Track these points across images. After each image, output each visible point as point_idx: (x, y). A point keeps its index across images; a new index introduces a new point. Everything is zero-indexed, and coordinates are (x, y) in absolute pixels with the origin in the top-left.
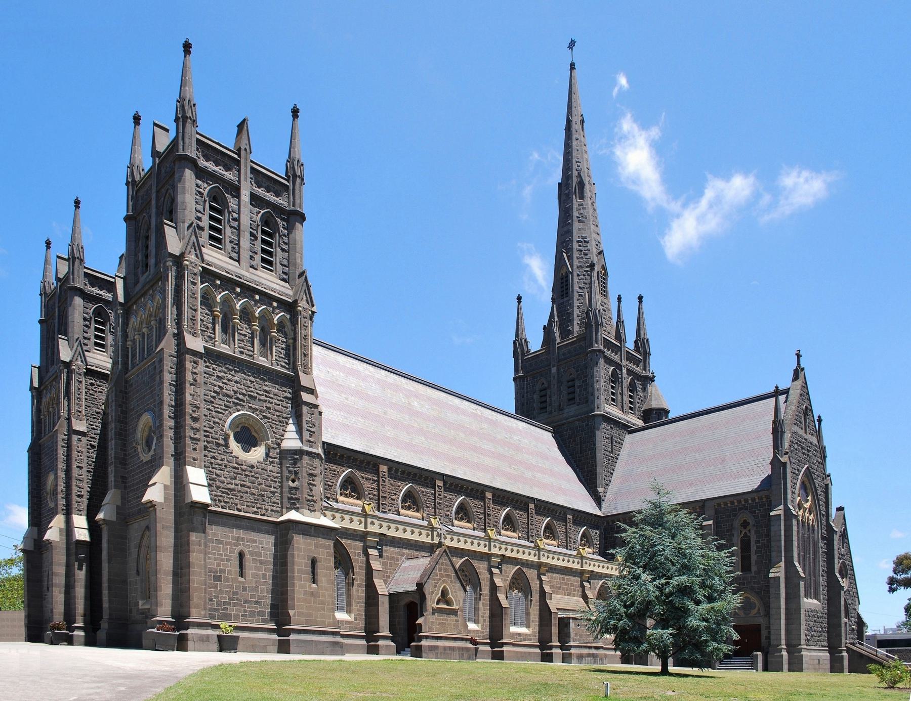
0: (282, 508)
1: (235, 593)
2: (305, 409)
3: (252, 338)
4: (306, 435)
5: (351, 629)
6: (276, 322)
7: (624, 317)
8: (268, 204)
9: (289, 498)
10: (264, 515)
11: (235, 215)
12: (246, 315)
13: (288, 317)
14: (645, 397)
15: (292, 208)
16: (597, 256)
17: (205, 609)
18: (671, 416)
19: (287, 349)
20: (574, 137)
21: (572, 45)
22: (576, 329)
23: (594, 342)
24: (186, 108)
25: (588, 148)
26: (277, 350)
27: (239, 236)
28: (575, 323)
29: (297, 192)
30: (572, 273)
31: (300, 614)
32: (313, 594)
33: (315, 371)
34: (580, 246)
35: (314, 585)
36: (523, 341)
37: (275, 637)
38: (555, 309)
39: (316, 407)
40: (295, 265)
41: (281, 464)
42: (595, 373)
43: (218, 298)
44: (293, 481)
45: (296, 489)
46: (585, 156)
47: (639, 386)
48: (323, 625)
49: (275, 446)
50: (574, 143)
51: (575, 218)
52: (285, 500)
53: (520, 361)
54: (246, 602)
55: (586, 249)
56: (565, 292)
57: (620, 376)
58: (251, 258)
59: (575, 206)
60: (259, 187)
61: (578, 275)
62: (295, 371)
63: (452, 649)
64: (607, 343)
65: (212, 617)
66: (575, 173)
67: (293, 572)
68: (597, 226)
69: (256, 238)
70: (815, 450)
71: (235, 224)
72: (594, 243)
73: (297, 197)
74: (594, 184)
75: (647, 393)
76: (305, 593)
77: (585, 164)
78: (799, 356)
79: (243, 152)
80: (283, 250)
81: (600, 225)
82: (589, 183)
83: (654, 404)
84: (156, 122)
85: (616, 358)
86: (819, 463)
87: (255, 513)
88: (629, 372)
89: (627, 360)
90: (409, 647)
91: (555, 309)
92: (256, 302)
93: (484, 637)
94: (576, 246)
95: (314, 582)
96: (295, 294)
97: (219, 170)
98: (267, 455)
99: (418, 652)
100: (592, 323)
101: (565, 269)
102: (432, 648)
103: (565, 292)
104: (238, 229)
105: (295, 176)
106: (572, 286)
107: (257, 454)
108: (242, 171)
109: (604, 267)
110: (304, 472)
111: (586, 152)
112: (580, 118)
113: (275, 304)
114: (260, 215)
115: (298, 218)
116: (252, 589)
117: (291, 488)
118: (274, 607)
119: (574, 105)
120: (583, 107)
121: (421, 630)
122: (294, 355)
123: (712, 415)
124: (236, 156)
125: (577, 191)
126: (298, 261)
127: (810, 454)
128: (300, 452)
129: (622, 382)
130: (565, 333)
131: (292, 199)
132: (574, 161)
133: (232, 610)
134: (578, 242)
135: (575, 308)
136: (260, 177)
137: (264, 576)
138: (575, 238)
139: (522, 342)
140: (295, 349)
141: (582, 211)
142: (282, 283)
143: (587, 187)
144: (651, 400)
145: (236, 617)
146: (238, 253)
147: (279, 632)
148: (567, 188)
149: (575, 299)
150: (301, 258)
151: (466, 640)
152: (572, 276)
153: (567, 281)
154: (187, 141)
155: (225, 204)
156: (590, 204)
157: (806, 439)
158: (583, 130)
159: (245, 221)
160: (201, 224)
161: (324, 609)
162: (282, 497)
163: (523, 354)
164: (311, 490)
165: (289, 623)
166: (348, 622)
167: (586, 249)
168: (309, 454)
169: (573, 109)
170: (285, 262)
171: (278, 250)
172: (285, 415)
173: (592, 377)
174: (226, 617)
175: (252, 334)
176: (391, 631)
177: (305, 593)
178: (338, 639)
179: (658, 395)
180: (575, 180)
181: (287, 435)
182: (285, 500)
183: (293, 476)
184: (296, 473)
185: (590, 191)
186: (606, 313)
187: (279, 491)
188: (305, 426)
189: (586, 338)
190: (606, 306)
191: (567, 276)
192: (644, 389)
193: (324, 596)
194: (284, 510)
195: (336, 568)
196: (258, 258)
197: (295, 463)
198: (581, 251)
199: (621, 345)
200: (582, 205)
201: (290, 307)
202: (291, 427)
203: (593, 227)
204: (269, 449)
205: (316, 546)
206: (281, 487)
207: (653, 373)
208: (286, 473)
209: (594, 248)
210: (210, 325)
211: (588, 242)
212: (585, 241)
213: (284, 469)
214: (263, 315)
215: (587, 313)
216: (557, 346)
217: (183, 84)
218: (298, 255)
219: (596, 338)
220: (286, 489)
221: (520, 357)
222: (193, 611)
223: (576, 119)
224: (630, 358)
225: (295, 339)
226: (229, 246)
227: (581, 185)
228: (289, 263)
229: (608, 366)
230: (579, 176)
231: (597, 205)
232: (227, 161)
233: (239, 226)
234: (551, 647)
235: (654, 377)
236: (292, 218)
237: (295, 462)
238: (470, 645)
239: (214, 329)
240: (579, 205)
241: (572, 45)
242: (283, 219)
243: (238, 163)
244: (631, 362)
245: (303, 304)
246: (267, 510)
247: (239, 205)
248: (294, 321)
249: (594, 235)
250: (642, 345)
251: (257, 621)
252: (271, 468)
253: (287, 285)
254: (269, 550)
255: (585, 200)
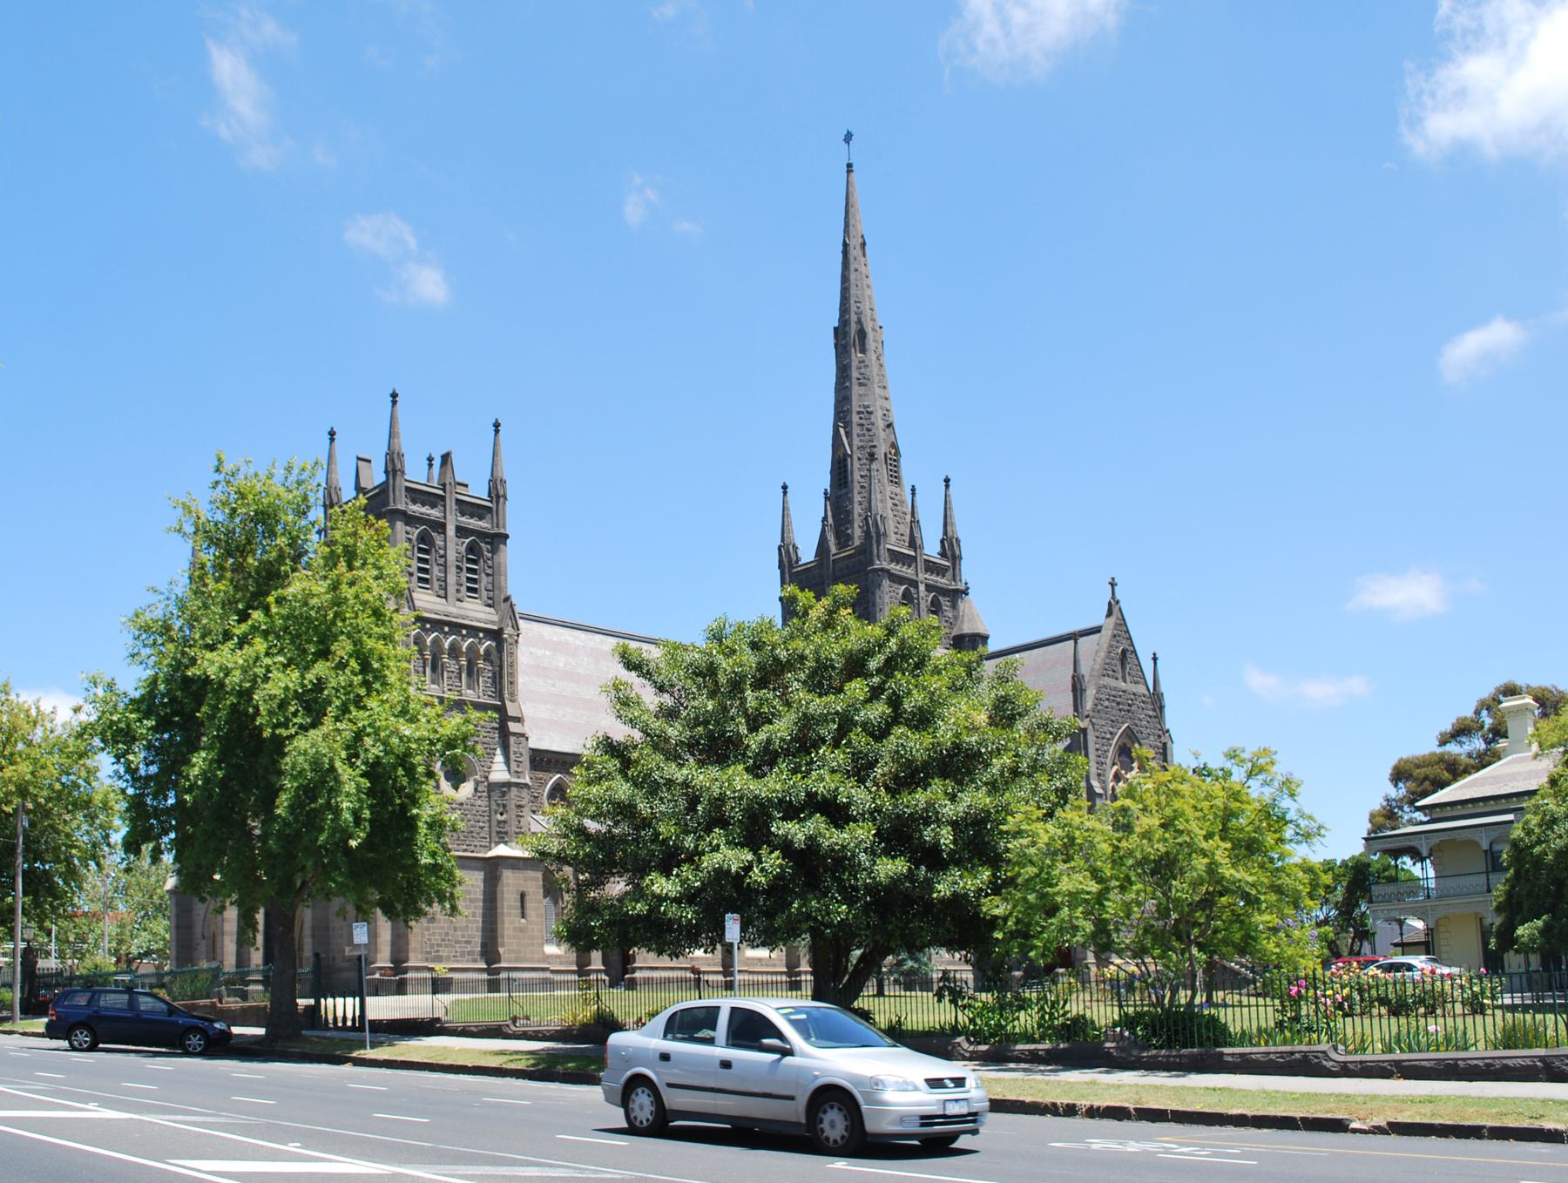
0: (490, 842)
1: (447, 934)
2: (512, 739)
3: (460, 674)
4: (514, 766)
5: (561, 963)
6: (482, 653)
7: (921, 516)
8: (471, 532)
9: (498, 833)
10: (473, 852)
11: (442, 552)
12: (454, 651)
13: (494, 644)
14: (956, 618)
15: (496, 531)
16: (884, 430)
17: (422, 953)
18: (992, 646)
19: (494, 677)
20: (852, 267)
21: (848, 138)
22: (857, 532)
23: (875, 558)
24: (396, 461)
25: (871, 281)
26: (484, 681)
27: (446, 572)
28: (856, 526)
29: (501, 512)
30: (851, 456)
31: (510, 951)
32: (522, 930)
33: (521, 697)
34: (861, 418)
35: (523, 921)
36: (791, 547)
37: (485, 976)
38: (829, 508)
39: (523, 735)
40: (500, 588)
41: (489, 797)
42: (878, 600)
43: (429, 641)
44: (502, 814)
45: (505, 822)
46: (868, 292)
47: (945, 602)
48: (532, 960)
49: (483, 779)
50: (853, 276)
51: (854, 381)
52: (494, 834)
53: (787, 576)
54: (457, 942)
55: (869, 422)
56: (843, 481)
57: (915, 596)
58: (458, 591)
59: (855, 364)
60: (463, 516)
61: (859, 459)
62: (503, 701)
63: (669, 981)
64: (896, 557)
65: (427, 960)
66: (854, 318)
67: (503, 908)
68: (884, 388)
69: (461, 569)
70: (1143, 702)
71: (441, 561)
72: (879, 413)
73: (501, 518)
74: (881, 327)
75: (958, 612)
76: (515, 929)
77: (868, 304)
78: (1113, 585)
79: (448, 487)
80: (488, 575)
81: (890, 386)
82: (873, 330)
83: (967, 629)
84: (360, 456)
85: (908, 572)
86: (1150, 717)
87: (465, 850)
88: (929, 588)
89: (927, 571)
90: (623, 980)
91: (829, 508)
92: (463, 636)
93: (714, 965)
94: (855, 418)
95: (523, 917)
96: (501, 620)
97: (425, 510)
98: (476, 790)
99: (632, 985)
100: (873, 534)
101: (842, 450)
102: (648, 982)
103: (843, 481)
104: (445, 565)
105: (498, 497)
106: (852, 474)
107: (467, 789)
108: (448, 507)
109: (894, 446)
110: (512, 806)
111: (868, 286)
112: (860, 240)
113: (481, 635)
114: (465, 545)
115: (502, 539)
116: (462, 929)
117: (499, 822)
118: (483, 945)
119: (852, 222)
120: (865, 224)
121: (634, 962)
122: (501, 683)
123: (1035, 651)
124: (441, 492)
125: (857, 342)
126: (503, 584)
127: (1133, 708)
128: (508, 785)
129: (918, 604)
130: (843, 538)
131: (495, 520)
132: (852, 302)
133: (444, 952)
134: (859, 413)
135: (856, 505)
136: (466, 508)
137: (474, 915)
138: (855, 408)
139: (789, 549)
140: (501, 677)
141: (863, 370)
142: (488, 609)
143: (870, 335)
144: (962, 622)
145: (448, 959)
146: (446, 589)
147: (489, 971)
148: (845, 338)
149: (856, 491)
150: (506, 580)
151: (686, 969)
152: (852, 459)
153: (846, 466)
154: (397, 493)
155: (431, 543)
156: (874, 358)
157: (1124, 691)
158: (864, 255)
159: (452, 556)
160: (410, 570)
161: (533, 944)
162: (490, 832)
163: (791, 566)
164: (519, 822)
165: (499, 961)
166: (558, 956)
167: (869, 422)
168: (517, 785)
169: (851, 228)
170: (490, 587)
171: (483, 575)
172: (492, 746)
173: (874, 604)
174: (439, 959)
175: (460, 669)
176: (604, 964)
177: (515, 929)
178: (548, 975)
179: (972, 614)
180: (854, 327)
181: (495, 767)
182: (494, 834)
183: (501, 810)
184: (504, 806)
185: (875, 341)
186: (899, 508)
187: (487, 825)
188: (512, 757)
189: (865, 553)
190: (898, 497)
191: (845, 460)
192: (954, 606)
193: (533, 930)
194: (493, 845)
195: (545, 897)
196: (463, 589)
197: (504, 796)
198: (862, 425)
199: (916, 552)
200: (863, 362)
201: (496, 635)
202: (499, 758)
203: (878, 391)
204: (477, 783)
205: (525, 880)
206: (490, 821)
207: (966, 584)
208: (494, 807)
209: (879, 420)
210: (421, 669)
211: (871, 413)
212: (868, 412)
213: (492, 802)
214: (470, 648)
215: (866, 519)
216: (832, 558)
217: (392, 434)
218: (502, 578)
219: (878, 553)
220: (494, 823)
221: (787, 570)
222: (411, 955)
223: (854, 243)
224: (931, 567)
225: (501, 667)
226: (436, 585)
227: (862, 334)
228: (494, 587)
229: (896, 586)
230: (859, 322)
231: (884, 360)
232: (432, 499)
233: (445, 562)
234: (799, 974)
235: (968, 588)
236: (496, 540)
237: (504, 794)
238: (689, 975)
239: (424, 673)
240: (860, 362)
241: (848, 138)
242: (487, 543)
243: (443, 498)
244: (932, 573)
245: (508, 631)
246: (476, 846)
247: (445, 541)
248: (500, 649)
249: (880, 402)
250: (950, 547)
251: (468, 961)
252: (479, 802)
253: (492, 610)
254: (478, 887)
255: (868, 354)
